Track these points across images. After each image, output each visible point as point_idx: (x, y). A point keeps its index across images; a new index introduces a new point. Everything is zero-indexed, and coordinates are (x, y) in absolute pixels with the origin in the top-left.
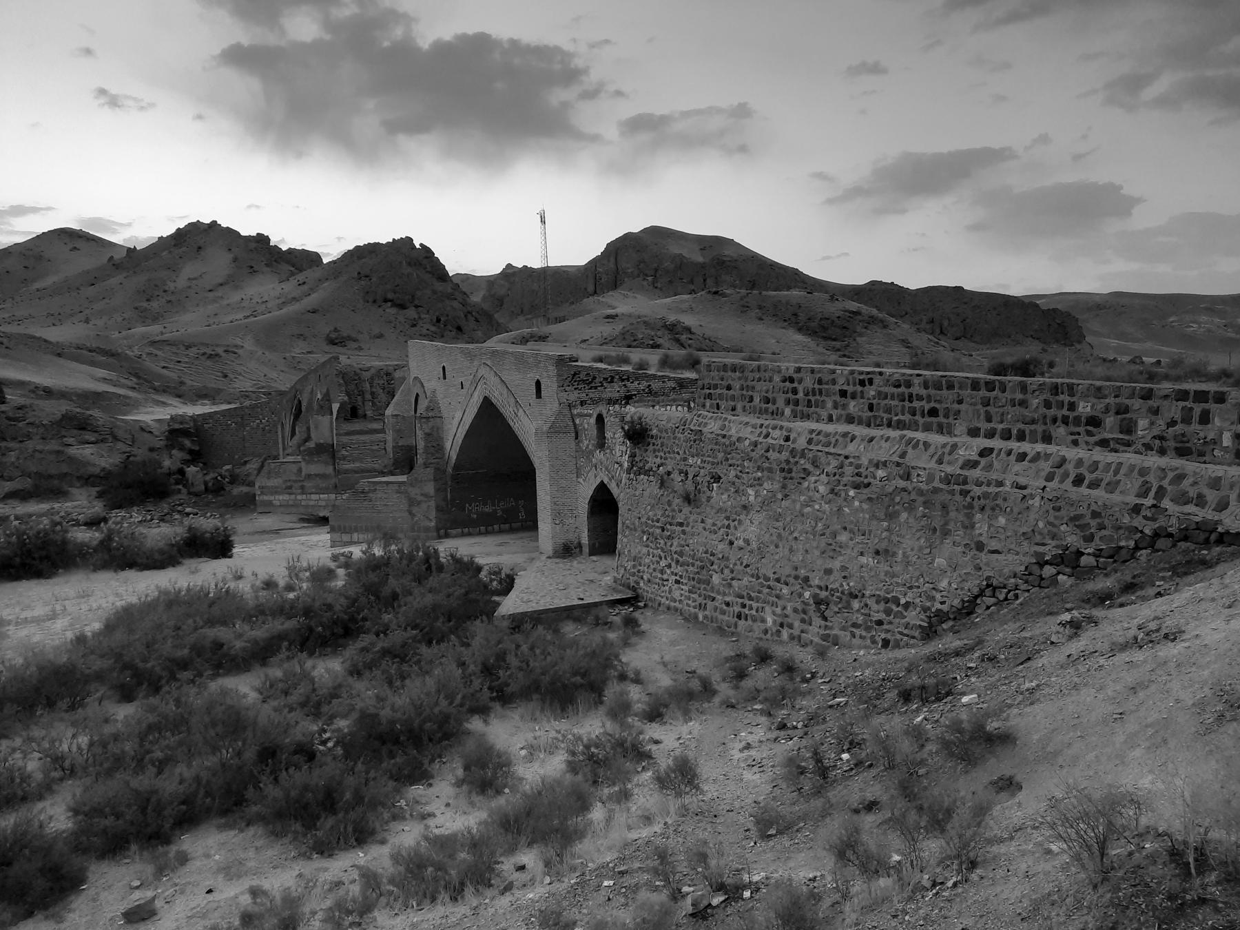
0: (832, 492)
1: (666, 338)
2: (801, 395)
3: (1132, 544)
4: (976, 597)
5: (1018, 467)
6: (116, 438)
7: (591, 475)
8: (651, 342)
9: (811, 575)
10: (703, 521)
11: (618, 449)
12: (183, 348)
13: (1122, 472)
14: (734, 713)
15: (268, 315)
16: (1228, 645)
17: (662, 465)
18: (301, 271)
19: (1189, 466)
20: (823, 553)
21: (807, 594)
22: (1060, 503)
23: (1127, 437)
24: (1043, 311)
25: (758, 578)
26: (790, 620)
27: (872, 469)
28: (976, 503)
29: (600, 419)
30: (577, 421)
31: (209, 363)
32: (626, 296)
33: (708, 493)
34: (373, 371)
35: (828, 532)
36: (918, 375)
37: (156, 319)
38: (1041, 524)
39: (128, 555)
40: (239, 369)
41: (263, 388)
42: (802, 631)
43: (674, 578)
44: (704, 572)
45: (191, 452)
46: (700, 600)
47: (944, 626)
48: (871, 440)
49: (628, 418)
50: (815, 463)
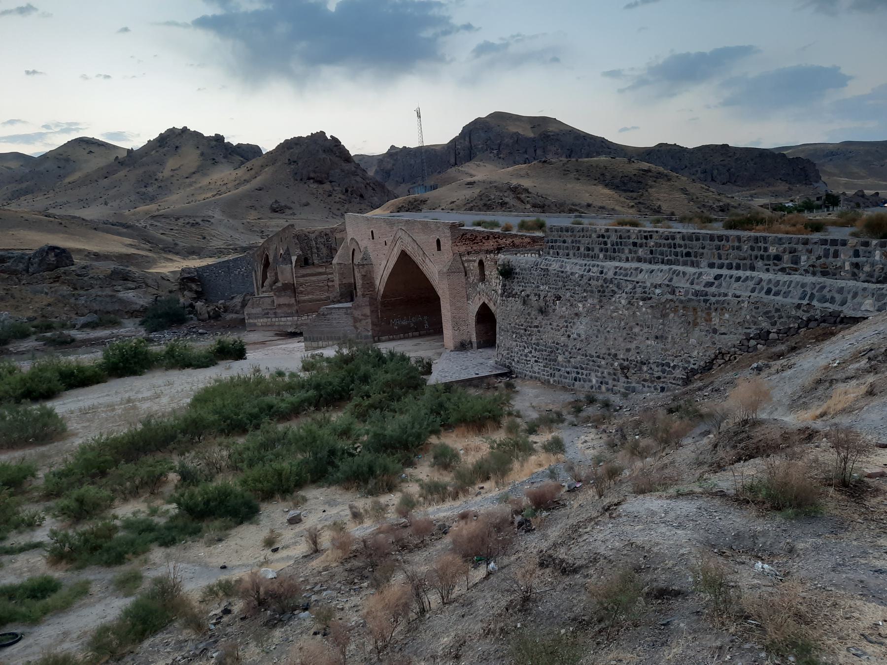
0: (629, 303)
1: (511, 197)
2: (609, 245)
3: (796, 325)
4: (713, 360)
5: (736, 285)
6: (147, 285)
7: (477, 299)
8: (501, 201)
9: (618, 353)
10: (551, 324)
11: (494, 282)
12: (174, 220)
13: (793, 285)
14: (577, 429)
15: (229, 193)
16: (813, 368)
17: (523, 291)
18: (248, 160)
19: (828, 281)
20: (625, 339)
21: (616, 364)
22: (759, 305)
23: (795, 266)
24: (789, 160)
25: (586, 356)
26: (606, 380)
27: (653, 289)
28: (712, 307)
29: (481, 263)
30: (466, 265)
31: (193, 229)
32: (478, 166)
33: (553, 307)
34: (317, 233)
35: (627, 327)
36: (679, 233)
37: (153, 199)
38: (748, 317)
39: (186, 360)
40: (212, 232)
41: (231, 245)
42: (614, 386)
43: (534, 359)
44: (553, 354)
45: (196, 292)
46: (551, 371)
47: (695, 377)
48: (652, 271)
49: (500, 262)
50: (618, 286)
